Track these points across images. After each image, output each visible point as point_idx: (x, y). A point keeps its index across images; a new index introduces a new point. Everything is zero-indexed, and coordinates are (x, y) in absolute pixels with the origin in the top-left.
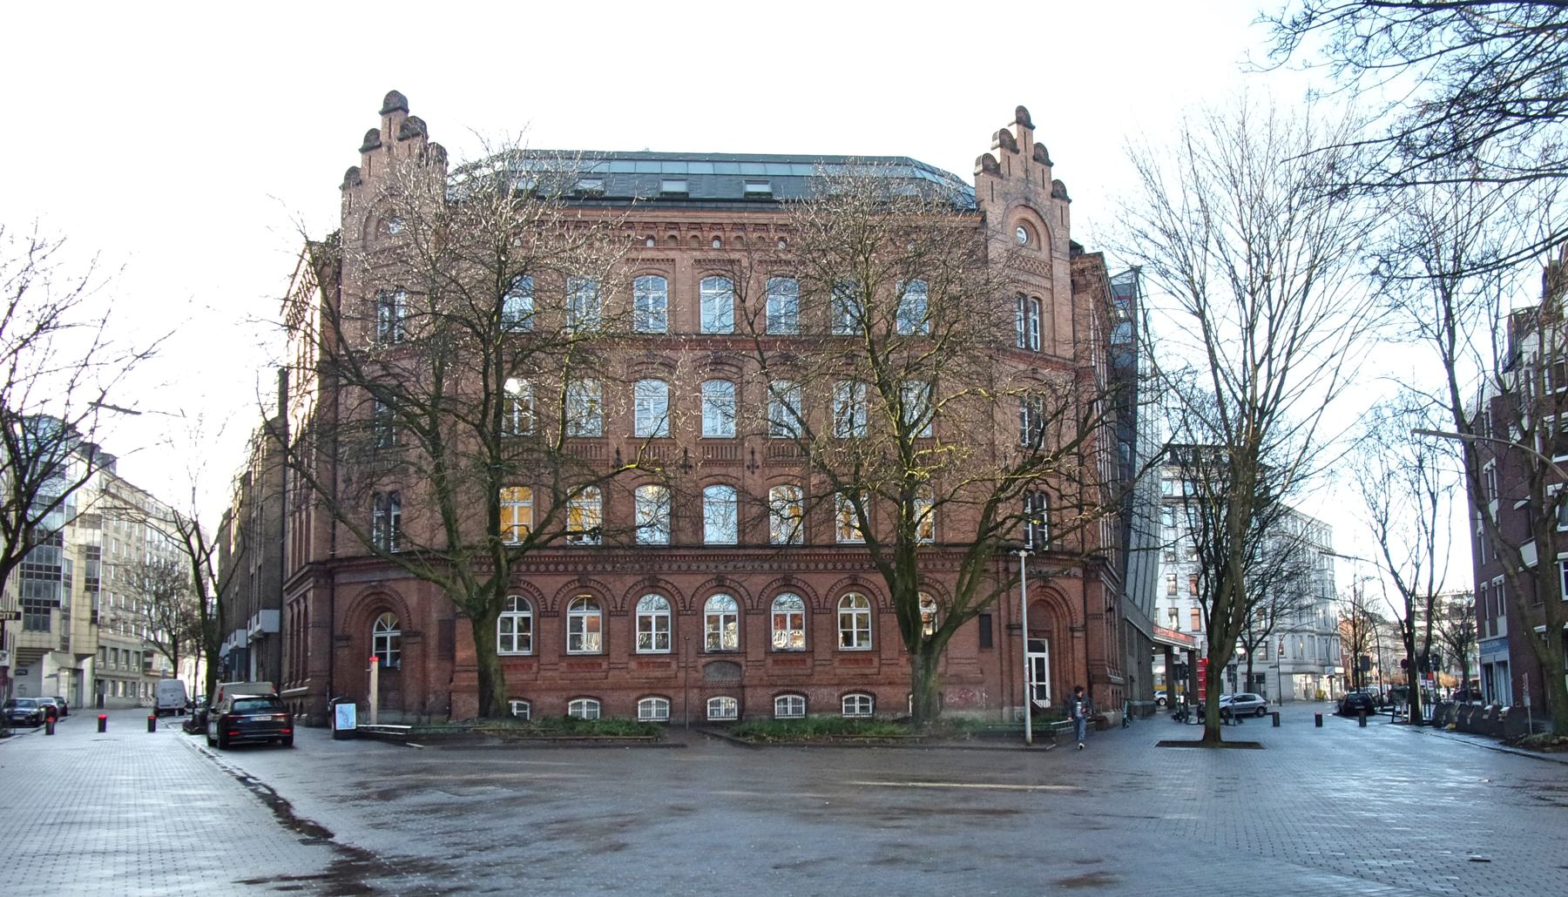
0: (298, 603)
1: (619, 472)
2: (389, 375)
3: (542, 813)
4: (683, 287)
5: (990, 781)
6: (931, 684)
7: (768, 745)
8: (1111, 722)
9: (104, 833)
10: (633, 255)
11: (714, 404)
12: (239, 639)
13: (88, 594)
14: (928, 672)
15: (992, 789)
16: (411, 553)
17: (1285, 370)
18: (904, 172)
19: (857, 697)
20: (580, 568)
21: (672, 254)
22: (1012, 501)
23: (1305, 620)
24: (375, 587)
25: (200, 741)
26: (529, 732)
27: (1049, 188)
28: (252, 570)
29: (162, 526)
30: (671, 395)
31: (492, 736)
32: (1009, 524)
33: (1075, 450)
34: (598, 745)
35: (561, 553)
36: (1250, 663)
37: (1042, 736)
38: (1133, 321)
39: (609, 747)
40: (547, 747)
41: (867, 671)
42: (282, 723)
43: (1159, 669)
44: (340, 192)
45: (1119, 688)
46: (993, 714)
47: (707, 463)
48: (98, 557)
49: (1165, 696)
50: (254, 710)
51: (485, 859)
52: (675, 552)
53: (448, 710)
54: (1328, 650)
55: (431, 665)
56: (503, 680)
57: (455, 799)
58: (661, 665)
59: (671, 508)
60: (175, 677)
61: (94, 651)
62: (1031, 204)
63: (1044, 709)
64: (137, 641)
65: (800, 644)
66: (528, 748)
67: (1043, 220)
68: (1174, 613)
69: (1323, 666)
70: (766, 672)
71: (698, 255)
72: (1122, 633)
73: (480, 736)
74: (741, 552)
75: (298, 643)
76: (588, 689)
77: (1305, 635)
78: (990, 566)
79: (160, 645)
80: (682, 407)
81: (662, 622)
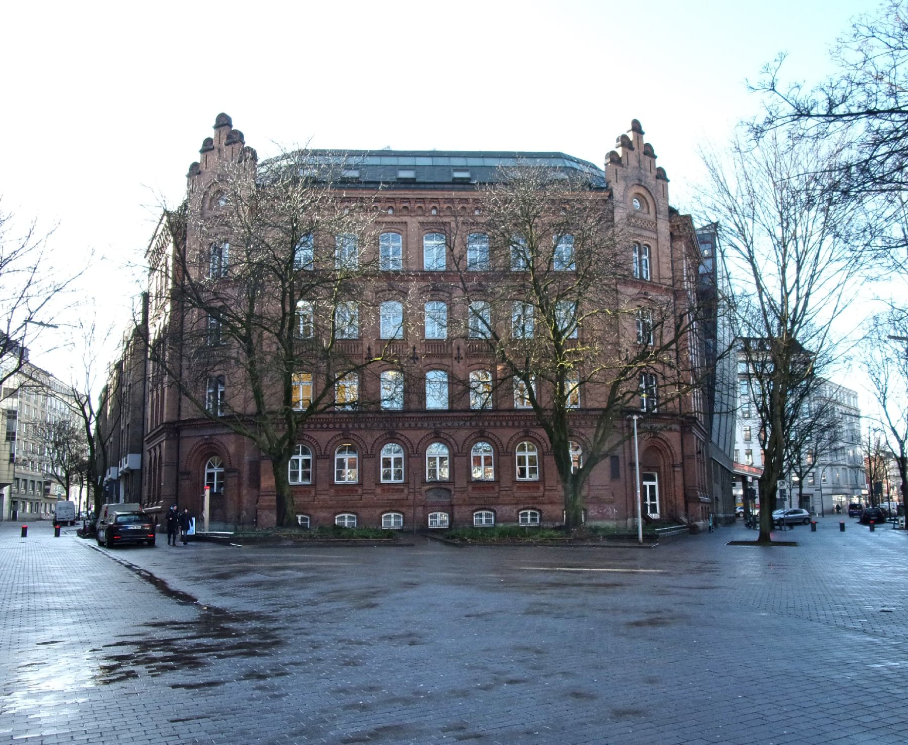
0: (155, 450)
1: (370, 363)
2: (217, 298)
3: (323, 586)
4: (413, 240)
5: (609, 567)
6: (578, 504)
7: (468, 545)
8: (701, 528)
9: (50, 599)
10: (380, 219)
11: (433, 318)
12: (112, 473)
13: (8, 443)
14: (575, 496)
15: (609, 572)
16: (231, 417)
17: (808, 295)
18: (559, 163)
19: (529, 512)
20: (344, 426)
21: (405, 219)
22: (631, 381)
23: (840, 458)
24: (207, 439)
25: (93, 543)
26: (311, 537)
27: (655, 173)
28: (122, 427)
29: (66, 399)
30: (404, 312)
31: (286, 539)
32: (629, 396)
33: (674, 346)
34: (355, 545)
35: (331, 416)
36: (801, 488)
37: (649, 538)
38: (713, 257)
39: (364, 546)
40: (322, 546)
41: (535, 495)
42: (148, 531)
43: (738, 492)
44: (186, 179)
45: (707, 506)
46: (622, 523)
47: (428, 356)
48: (15, 418)
49: (743, 510)
50: (129, 522)
51: (293, 612)
52: (408, 415)
53: (255, 521)
54: (856, 478)
55: (244, 492)
56: (293, 501)
57: (268, 578)
58: (398, 491)
59: (405, 387)
60: (68, 499)
61: (11, 482)
62: (643, 184)
63: (655, 520)
64: (39, 474)
65: (491, 476)
66: (310, 546)
67: (651, 194)
68: (749, 453)
69: (853, 489)
70: (468, 495)
71: (421, 219)
72: (709, 468)
73: (279, 539)
74: (451, 414)
75: (155, 476)
76: (348, 508)
77: (840, 468)
78: (618, 424)
79: (57, 477)
80: (411, 319)
81: (398, 461)
